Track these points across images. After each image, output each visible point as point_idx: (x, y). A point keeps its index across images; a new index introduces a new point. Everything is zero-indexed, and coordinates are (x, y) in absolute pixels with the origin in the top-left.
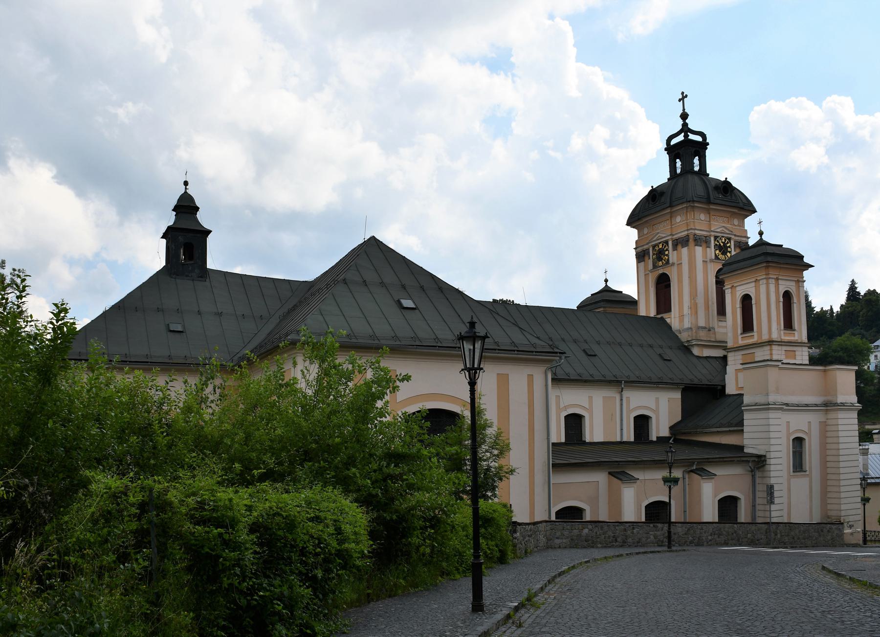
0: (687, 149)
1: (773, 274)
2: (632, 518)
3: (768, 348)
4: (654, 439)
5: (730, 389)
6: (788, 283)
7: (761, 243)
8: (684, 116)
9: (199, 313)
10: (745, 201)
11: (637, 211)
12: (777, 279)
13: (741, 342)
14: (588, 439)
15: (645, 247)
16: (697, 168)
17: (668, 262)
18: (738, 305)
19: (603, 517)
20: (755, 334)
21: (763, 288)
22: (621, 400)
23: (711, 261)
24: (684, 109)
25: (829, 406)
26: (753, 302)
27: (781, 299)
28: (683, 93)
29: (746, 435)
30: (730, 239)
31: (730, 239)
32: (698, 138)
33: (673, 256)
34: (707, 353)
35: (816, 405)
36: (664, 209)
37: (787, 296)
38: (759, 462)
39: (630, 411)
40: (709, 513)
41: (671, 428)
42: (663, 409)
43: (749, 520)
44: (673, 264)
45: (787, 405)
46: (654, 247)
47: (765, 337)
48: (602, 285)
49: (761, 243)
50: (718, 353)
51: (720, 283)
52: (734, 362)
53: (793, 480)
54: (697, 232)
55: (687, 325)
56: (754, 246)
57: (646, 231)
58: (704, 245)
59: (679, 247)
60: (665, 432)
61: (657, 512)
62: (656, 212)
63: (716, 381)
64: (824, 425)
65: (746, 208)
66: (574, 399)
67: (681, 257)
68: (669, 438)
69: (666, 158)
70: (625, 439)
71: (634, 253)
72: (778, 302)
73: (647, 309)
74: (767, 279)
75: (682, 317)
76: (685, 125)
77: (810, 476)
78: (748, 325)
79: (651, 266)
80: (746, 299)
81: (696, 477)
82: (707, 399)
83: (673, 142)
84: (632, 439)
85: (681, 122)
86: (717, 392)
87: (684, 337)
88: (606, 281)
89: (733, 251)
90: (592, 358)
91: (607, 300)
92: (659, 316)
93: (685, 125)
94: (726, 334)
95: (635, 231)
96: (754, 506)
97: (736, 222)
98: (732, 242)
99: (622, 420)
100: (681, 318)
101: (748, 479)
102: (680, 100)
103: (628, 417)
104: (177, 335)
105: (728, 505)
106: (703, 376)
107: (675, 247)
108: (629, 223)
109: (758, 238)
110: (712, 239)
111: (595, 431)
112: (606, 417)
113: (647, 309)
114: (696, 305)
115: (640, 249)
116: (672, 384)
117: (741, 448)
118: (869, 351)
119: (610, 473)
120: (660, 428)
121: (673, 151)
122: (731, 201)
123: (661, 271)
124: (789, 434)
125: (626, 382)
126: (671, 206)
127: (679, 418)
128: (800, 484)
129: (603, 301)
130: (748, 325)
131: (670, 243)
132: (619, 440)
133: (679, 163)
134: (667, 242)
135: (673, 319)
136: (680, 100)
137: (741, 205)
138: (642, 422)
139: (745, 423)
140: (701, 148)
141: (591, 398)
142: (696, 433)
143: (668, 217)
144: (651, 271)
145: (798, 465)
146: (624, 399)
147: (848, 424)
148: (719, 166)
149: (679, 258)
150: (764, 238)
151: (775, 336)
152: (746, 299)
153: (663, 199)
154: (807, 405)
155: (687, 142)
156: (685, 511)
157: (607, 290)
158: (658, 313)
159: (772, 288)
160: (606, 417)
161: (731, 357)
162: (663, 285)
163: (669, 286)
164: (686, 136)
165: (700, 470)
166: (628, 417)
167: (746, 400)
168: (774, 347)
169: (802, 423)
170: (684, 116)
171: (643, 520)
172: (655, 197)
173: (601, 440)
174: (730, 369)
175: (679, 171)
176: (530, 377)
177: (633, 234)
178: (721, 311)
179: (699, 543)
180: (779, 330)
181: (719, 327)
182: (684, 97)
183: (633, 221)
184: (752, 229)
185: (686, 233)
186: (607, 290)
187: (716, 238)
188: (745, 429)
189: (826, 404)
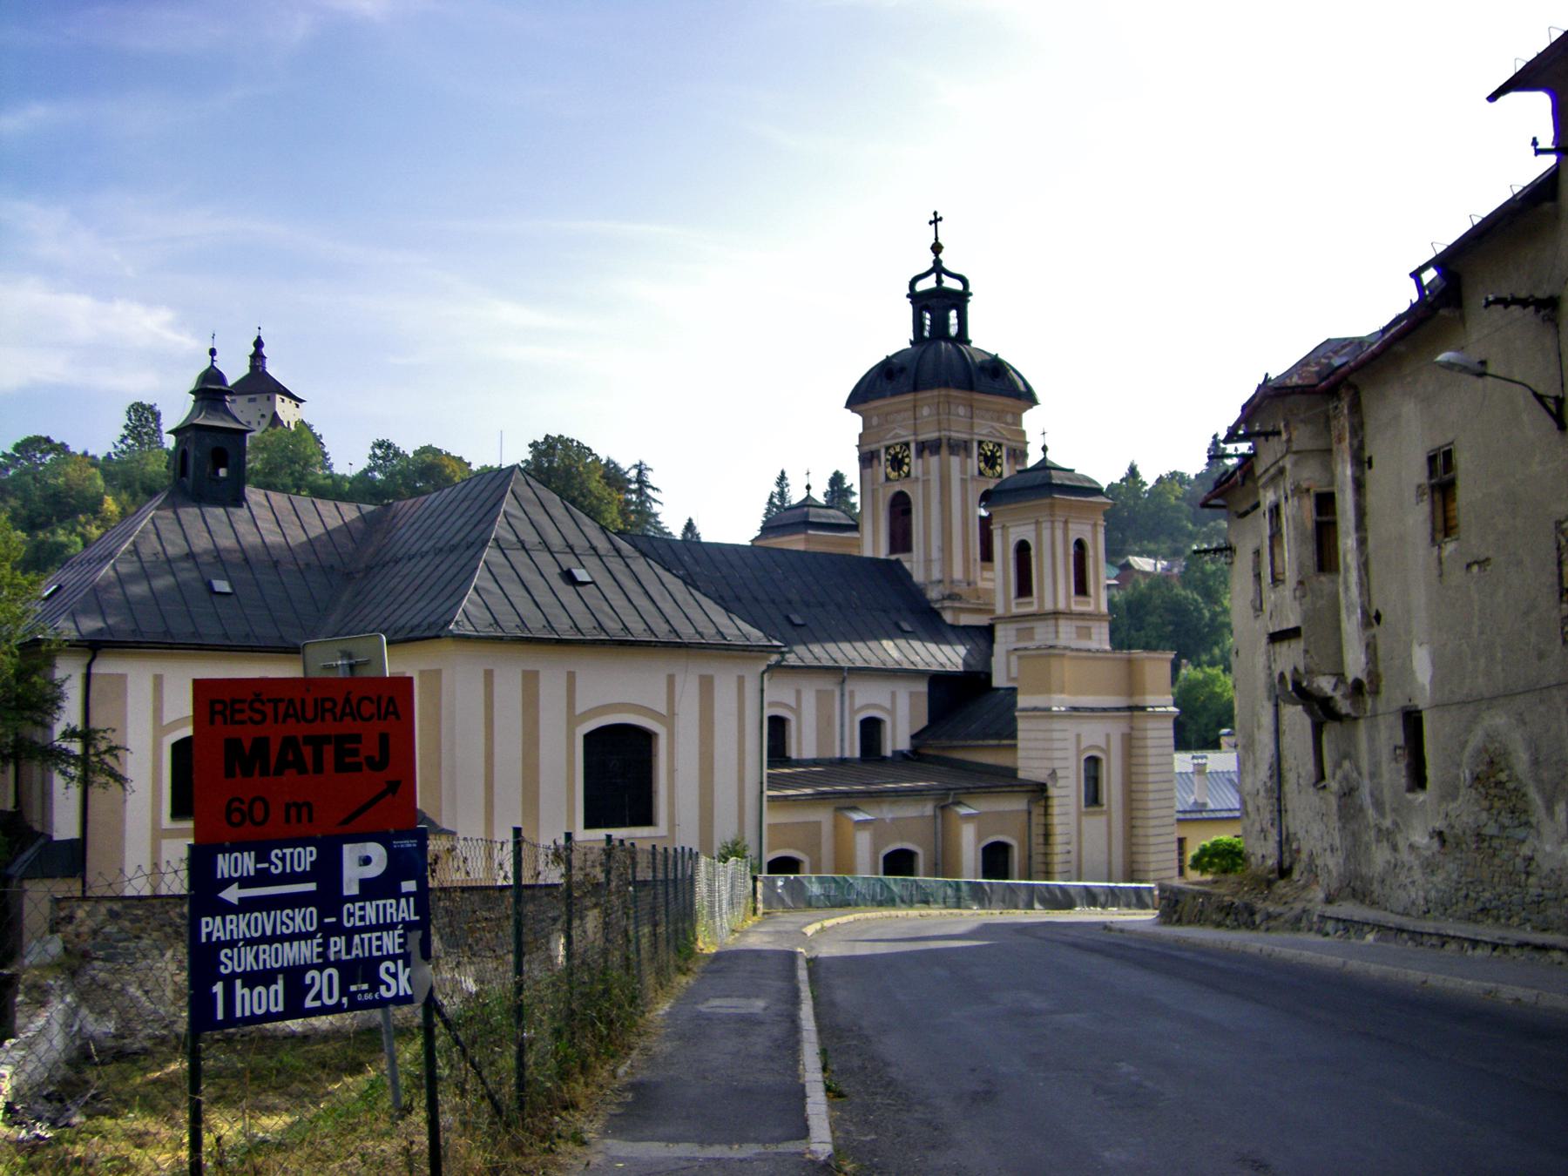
0: (938, 303)
5: (999, 681)
7: (1044, 466)
8: (937, 248)
11: (864, 385)
13: (1015, 610)
16: (953, 330)
17: (908, 475)
21: (1046, 534)
22: (842, 695)
23: (973, 478)
26: (1033, 552)
29: (1020, 753)
30: (1000, 445)
31: (1000, 445)
33: (915, 465)
38: (1039, 792)
39: (854, 712)
41: (913, 737)
46: (887, 448)
47: (1049, 606)
49: (1044, 466)
50: (982, 620)
53: (1085, 820)
55: (936, 574)
56: (1034, 468)
58: (962, 453)
59: (926, 453)
60: (904, 744)
70: (847, 755)
71: (857, 454)
75: (928, 561)
76: (937, 262)
77: (1108, 813)
78: (1024, 588)
83: (921, 286)
84: (857, 754)
85: (932, 257)
89: (1006, 469)
92: (893, 557)
93: (937, 262)
103: (852, 721)
107: (920, 453)
110: (975, 445)
111: (804, 744)
115: (866, 448)
117: (1011, 772)
118: (1119, 906)
120: (897, 738)
121: (919, 301)
122: (1000, 384)
123: (897, 487)
124: (1079, 752)
127: (923, 722)
128: (1095, 826)
130: (1024, 588)
131: (913, 446)
132: (838, 755)
134: (907, 445)
138: (871, 729)
140: (959, 300)
141: (798, 693)
145: (1093, 797)
146: (847, 697)
147: (1162, 733)
148: (988, 331)
149: (926, 472)
150: (1050, 456)
151: (1061, 606)
152: (1023, 549)
158: (893, 550)
159: (1059, 534)
161: (1000, 632)
162: (900, 507)
164: (939, 281)
166: (852, 721)
167: (1023, 701)
168: (1062, 622)
169: (1100, 735)
170: (937, 248)
174: (999, 649)
175: (926, 334)
176: (741, 680)
177: (855, 423)
178: (987, 555)
180: (1068, 597)
181: (983, 579)
182: (936, 220)
187: (980, 443)
188: (1020, 744)
189: (1130, 708)
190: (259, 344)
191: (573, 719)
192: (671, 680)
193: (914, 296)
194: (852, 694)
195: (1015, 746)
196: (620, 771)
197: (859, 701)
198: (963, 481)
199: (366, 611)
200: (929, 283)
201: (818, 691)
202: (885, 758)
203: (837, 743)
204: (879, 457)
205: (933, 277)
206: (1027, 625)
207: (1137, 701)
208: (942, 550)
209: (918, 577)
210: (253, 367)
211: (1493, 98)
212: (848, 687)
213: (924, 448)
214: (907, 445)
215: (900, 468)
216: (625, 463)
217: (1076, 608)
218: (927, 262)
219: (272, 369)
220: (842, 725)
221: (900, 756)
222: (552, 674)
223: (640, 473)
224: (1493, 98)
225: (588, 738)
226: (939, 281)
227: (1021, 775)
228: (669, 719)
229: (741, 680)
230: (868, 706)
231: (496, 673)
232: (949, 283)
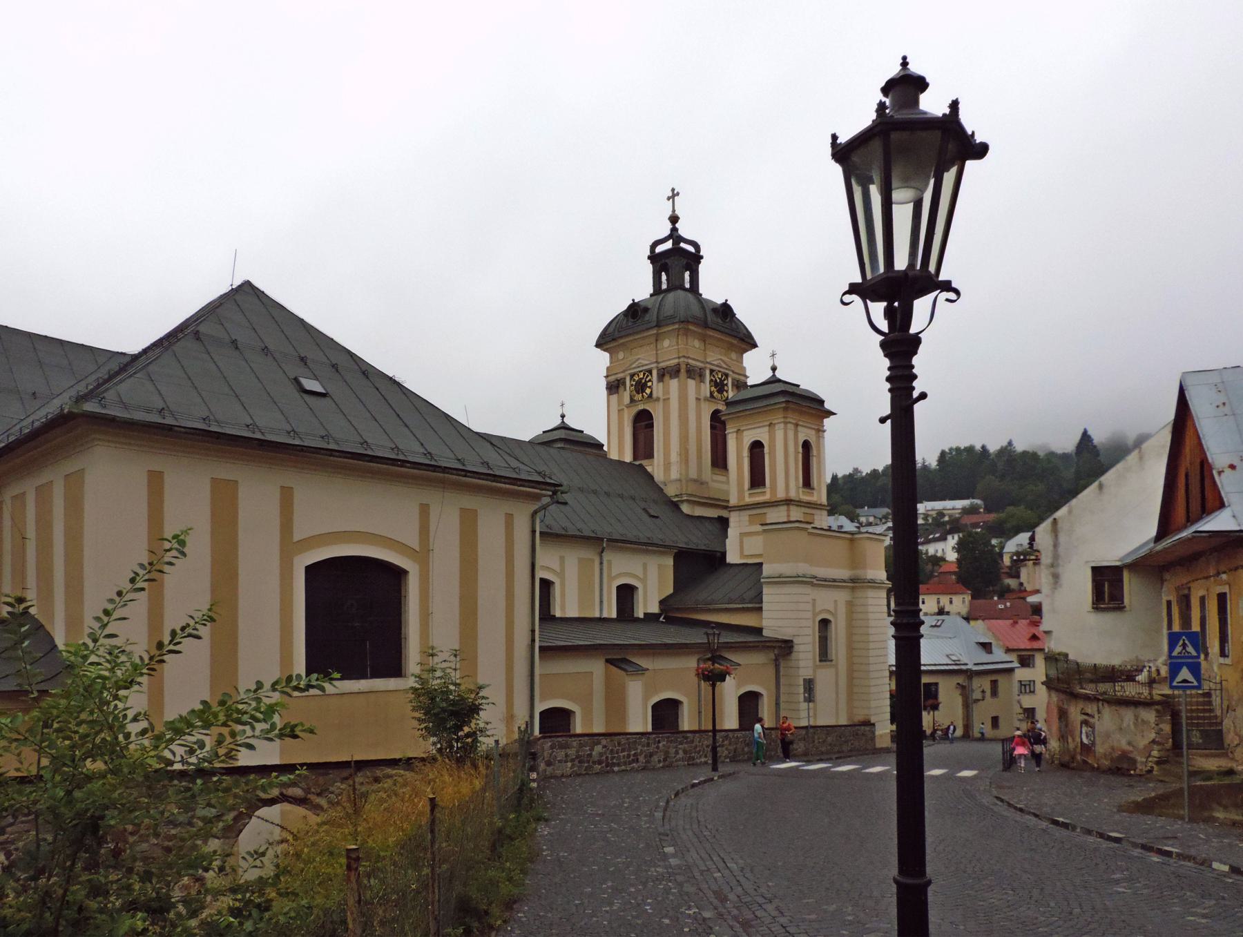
0: (676, 260)
1: (792, 417)
2: (639, 729)
3: (784, 508)
4: (641, 616)
6: (809, 431)
8: (674, 219)
12: (797, 425)
14: (558, 614)
15: (620, 376)
16: (687, 286)
17: (650, 396)
21: (779, 434)
22: (601, 563)
23: (706, 399)
24: (674, 211)
25: (856, 583)
26: (766, 450)
27: (801, 450)
28: (673, 190)
29: (765, 614)
30: (727, 375)
32: (691, 249)
33: (657, 388)
34: (699, 511)
35: (844, 581)
36: (648, 329)
37: (806, 445)
39: (611, 579)
41: (661, 602)
42: (654, 582)
44: (658, 399)
46: (632, 376)
47: (781, 495)
48: (557, 422)
52: (738, 525)
54: (690, 361)
57: (621, 355)
59: (667, 378)
62: (637, 333)
63: (715, 547)
64: (850, 604)
65: (748, 342)
68: (659, 615)
69: (649, 268)
70: (605, 615)
72: (797, 452)
73: (620, 450)
74: (786, 423)
75: (667, 466)
76: (674, 230)
77: (836, 667)
78: (757, 479)
79: (627, 400)
80: (757, 447)
83: (659, 249)
84: (614, 615)
85: (670, 226)
86: (715, 560)
87: (671, 491)
88: (563, 416)
91: (566, 439)
93: (674, 230)
94: (727, 492)
95: (607, 355)
96: (777, 704)
97: (734, 356)
101: (771, 671)
102: (669, 199)
106: (697, 540)
107: (661, 377)
108: (600, 344)
109: (771, 374)
110: (708, 372)
111: (567, 605)
112: (582, 589)
113: (620, 450)
114: (687, 451)
115: (612, 378)
116: (665, 546)
119: (607, 661)
120: (647, 604)
121: (658, 261)
122: (725, 327)
123: (641, 407)
124: (815, 615)
125: (610, 540)
126: (658, 325)
129: (561, 440)
130: (757, 479)
131: (655, 373)
132: (597, 615)
133: (664, 277)
134: (650, 372)
135: (655, 468)
136: (669, 199)
137: (741, 335)
138: (626, 593)
139: (765, 598)
140: (693, 260)
141: (562, 559)
143: (653, 339)
144: (628, 406)
145: (824, 654)
146: (605, 563)
148: (714, 285)
149: (666, 392)
151: (793, 495)
152: (757, 447)
153: (647, 317)
154: (834, 581)
155: (676, 251)
156: (700, 712)
157: (564, 427)
159: (791, 434)
160: (582, 589)
161: (734, 519)
162: (643, 422)
167: (767, 570)
168: (793, 508)
170: (674, 219)
172: (635, 311)
173: (576, 615)
176: (509, 518)
177: (603, 359)
182: (674, 195)
183: (606, 340)
184: (755, 368)
186: (564, 427)
187: (712, 371)
189: (853, 580)
192: (424, 510)
193: (654, 258)
194: (610, 562)
195: (760, 609)
198: (698, 399)
202: (638, 619)
204: (624, 384)
207: (859, 573)
209: (659, 476)
212: (607, 556)
215: (643, 391)
217: (806, 498)
218: (666, 230)
220: (601, 590)
221: (650, 618)
222: (258, 493)
228: (423, 555)
229: (509, 518)
231: (168, 479)
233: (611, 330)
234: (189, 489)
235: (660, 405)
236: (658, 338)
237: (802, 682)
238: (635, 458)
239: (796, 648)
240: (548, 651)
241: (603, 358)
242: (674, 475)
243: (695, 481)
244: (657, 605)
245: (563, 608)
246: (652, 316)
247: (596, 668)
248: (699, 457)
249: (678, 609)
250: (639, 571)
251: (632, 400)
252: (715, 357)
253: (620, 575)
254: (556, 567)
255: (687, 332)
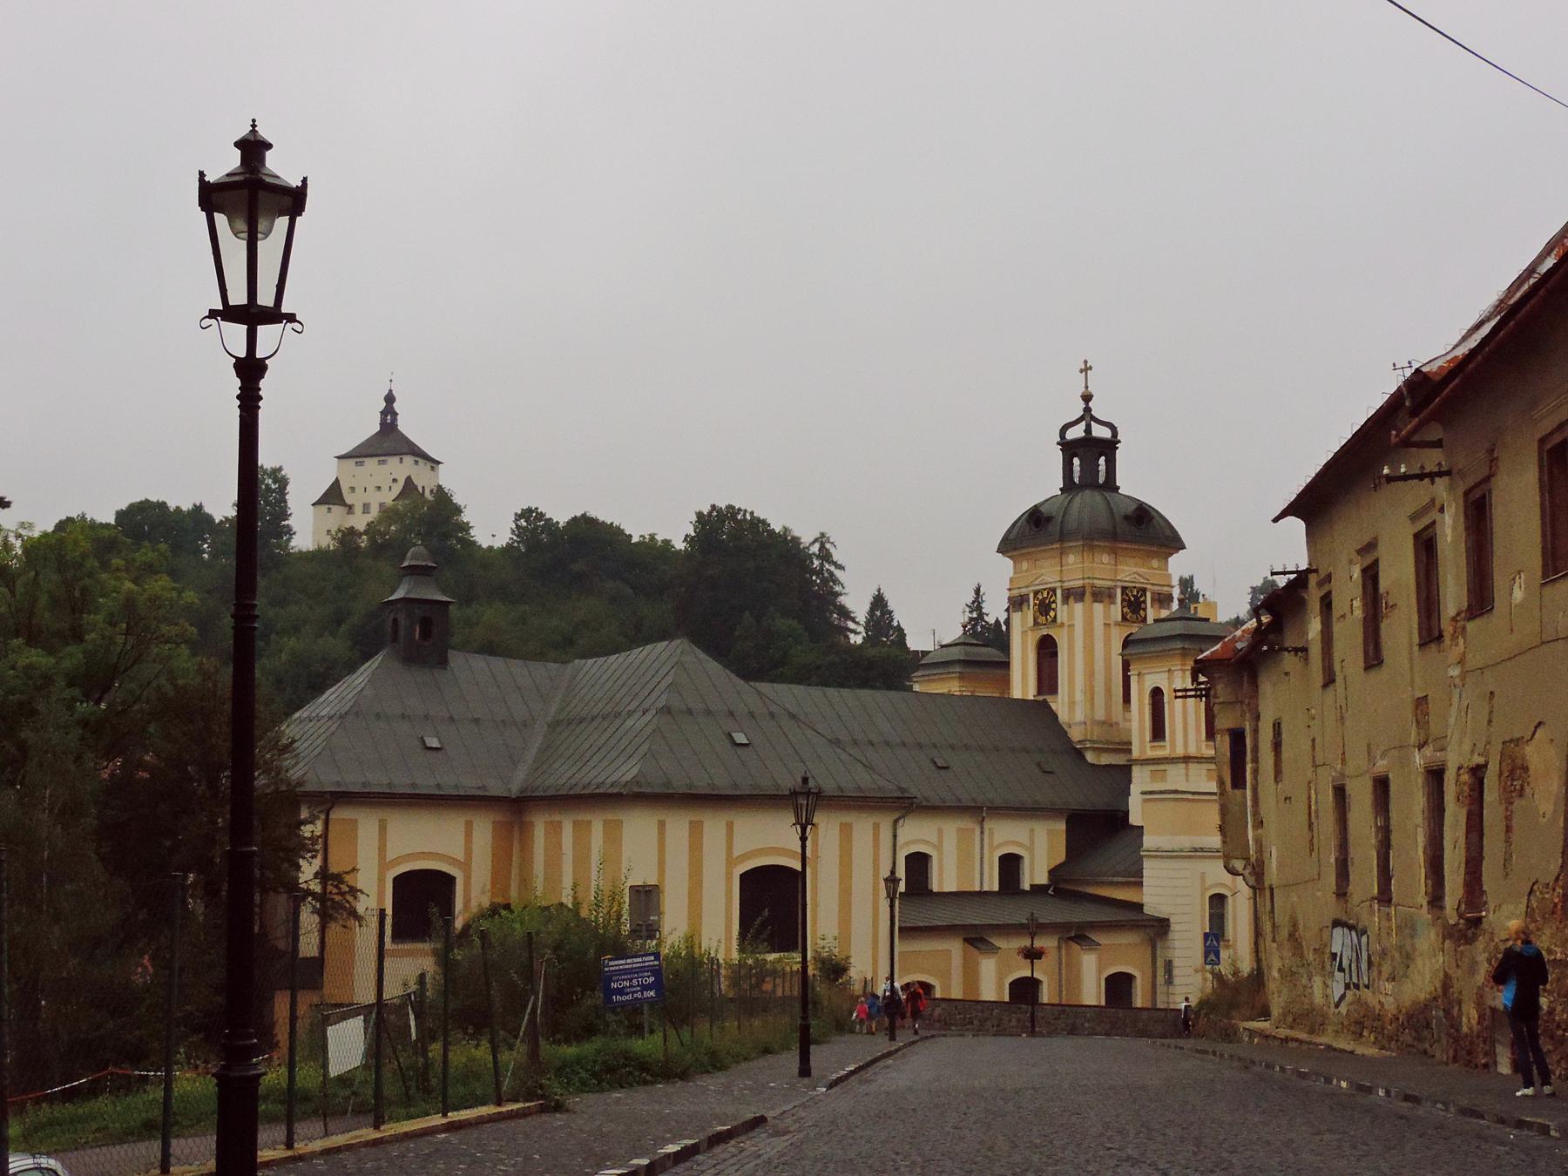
0: (1090, 453)
4: (1027, 887)
9: (451, 719)
10: (1168, 532)
13: (1150, 754)
14: (935, 889)
15: (1024, 591)
16: (1101, 480)
18: (1147, 700)
19: (956, 993)
20: (1167, 743)
23: (1117, 624)
31: (1144, 590)
33: (1061, 611)
34: (1106, 759)
38: (1160, 927)
39: (993, 848)
40: (1092, 993)
41: (1052, 872)
42: (1041, 848)
43: (1148, 1005)
45: (1202, 850)
46: (1036, 593)
47: (1180, 752)
50: (1120, 760)
51: (1126, 667)
52: (1141, 780)
59: (1071, 600)
60: (1042, 879)
61: (1025, 990)
65: (1170, 542)
66: (917, 834)
67: (1072, 615)
75: (1072, 704)
76: (1087, 410)
78: (1158, 732)
81: (1075, 947)
82: (1100, 829)
84: (996, 888)
85: (1082, 405)
87: (1076, 734)
90: (943, 772)
92: (1041, 698)
93: (1087, 410)
98: (1149, 595)
99: (982, 874)
100: (1073, 707)
103: (991, 863)
104: (434, 754)
105: (1118, 986)
107: (1066, 599)
110: (1119, 591)
111: (944, 878)
112: (960, 857)
114: (1092, 688)
115: (1015, 592)
120: (1035, 873)
121: (1070, 449)
122: (1147, 531)
124: (1204, 890)
125: (989, 808)
127: (1061, 857)
130: (1158, 732)
131: (1059, 592)
133: (1076, 461)
134: (1054, 590)
135: (1059, 705)
138: (1010, 865)
140: (1108, 447)
141: (940, 831)
142: (1088, 883)
146: (986, 833)
148: (1135, 479)
149: (1071, 616)
151: (1192, 751)
152: (1157, 693)
153: (1050, 528)
160: (960, 857)
161: (1136, 772)
163: (1055, 654)
164: (1088, 430)
165: (1078, 935)
168: (1192, 766)
170: (1087, 398)
171: (1007, 999)
173: (954, 889)
174: (1135, 789)
176: (876, 827)
179: (1073, 1031)
180: (1198, 741)
182: (1086, 369)
183: (1011, 544)
185: (1080, 583)
187: (1124, 589)
190: (390, 399)
191: (731, 862)
195: (1141, 884)
196: (773, 900)
197: (998, 839)
198: (1107, 625)
199: (555, 766)
200: (1076, 433)
201: (959, 830)
202: (1025, 892)
203: (977, 876)
205: (1083, 425)
206: (1162, 767)
208: (406, 1134)
209: (1063, 716)
210: (383, 424)
211: (1276, 520)
213: (1072, 595)
214: (1054, 590)
216: (806, 535)
219: (403, 426)
221: (1037, 890)
222: (714, 825)
223: (822, 547)
224: (1276, 520)
225: (745, 877)
226: (1088, 430)
227: (1146, 910)
230: (1006, 843)
232: (1100, 432)
233: (1012, 536)
234: (678, 825)
235: (1065, 630)
236: (1063, 553)
237: (627, 891)
238: (1039, 692)
239: (1173, 927)
240: (909, 932)
241: (1006, 565)
242: (1079, 716)
243: (1104, 723)
244: (1045, 875)
245: (941, 883)
246: (1054, 528)
247: (955, 948)
248: (1108, 691)
249: (1066, 881)
250: (1025, 839)
251: (1036, 623)
252: (1130, 571)
253: (1000, 845)
254: (935, 840)
255: (1092, 548)
